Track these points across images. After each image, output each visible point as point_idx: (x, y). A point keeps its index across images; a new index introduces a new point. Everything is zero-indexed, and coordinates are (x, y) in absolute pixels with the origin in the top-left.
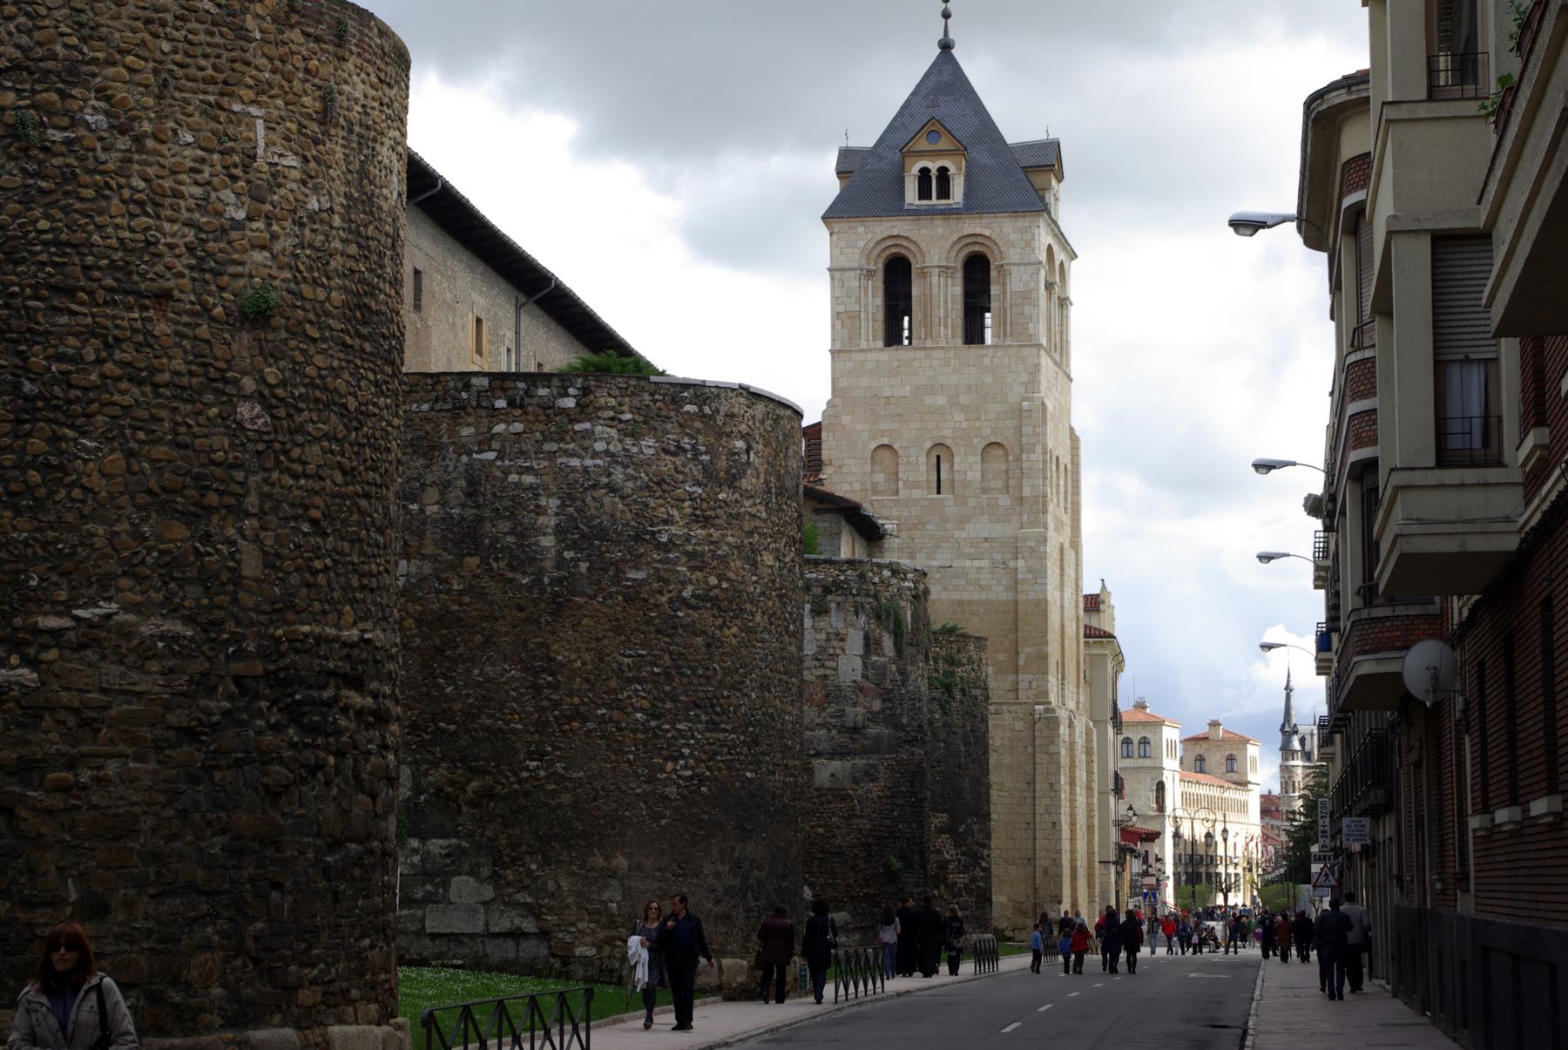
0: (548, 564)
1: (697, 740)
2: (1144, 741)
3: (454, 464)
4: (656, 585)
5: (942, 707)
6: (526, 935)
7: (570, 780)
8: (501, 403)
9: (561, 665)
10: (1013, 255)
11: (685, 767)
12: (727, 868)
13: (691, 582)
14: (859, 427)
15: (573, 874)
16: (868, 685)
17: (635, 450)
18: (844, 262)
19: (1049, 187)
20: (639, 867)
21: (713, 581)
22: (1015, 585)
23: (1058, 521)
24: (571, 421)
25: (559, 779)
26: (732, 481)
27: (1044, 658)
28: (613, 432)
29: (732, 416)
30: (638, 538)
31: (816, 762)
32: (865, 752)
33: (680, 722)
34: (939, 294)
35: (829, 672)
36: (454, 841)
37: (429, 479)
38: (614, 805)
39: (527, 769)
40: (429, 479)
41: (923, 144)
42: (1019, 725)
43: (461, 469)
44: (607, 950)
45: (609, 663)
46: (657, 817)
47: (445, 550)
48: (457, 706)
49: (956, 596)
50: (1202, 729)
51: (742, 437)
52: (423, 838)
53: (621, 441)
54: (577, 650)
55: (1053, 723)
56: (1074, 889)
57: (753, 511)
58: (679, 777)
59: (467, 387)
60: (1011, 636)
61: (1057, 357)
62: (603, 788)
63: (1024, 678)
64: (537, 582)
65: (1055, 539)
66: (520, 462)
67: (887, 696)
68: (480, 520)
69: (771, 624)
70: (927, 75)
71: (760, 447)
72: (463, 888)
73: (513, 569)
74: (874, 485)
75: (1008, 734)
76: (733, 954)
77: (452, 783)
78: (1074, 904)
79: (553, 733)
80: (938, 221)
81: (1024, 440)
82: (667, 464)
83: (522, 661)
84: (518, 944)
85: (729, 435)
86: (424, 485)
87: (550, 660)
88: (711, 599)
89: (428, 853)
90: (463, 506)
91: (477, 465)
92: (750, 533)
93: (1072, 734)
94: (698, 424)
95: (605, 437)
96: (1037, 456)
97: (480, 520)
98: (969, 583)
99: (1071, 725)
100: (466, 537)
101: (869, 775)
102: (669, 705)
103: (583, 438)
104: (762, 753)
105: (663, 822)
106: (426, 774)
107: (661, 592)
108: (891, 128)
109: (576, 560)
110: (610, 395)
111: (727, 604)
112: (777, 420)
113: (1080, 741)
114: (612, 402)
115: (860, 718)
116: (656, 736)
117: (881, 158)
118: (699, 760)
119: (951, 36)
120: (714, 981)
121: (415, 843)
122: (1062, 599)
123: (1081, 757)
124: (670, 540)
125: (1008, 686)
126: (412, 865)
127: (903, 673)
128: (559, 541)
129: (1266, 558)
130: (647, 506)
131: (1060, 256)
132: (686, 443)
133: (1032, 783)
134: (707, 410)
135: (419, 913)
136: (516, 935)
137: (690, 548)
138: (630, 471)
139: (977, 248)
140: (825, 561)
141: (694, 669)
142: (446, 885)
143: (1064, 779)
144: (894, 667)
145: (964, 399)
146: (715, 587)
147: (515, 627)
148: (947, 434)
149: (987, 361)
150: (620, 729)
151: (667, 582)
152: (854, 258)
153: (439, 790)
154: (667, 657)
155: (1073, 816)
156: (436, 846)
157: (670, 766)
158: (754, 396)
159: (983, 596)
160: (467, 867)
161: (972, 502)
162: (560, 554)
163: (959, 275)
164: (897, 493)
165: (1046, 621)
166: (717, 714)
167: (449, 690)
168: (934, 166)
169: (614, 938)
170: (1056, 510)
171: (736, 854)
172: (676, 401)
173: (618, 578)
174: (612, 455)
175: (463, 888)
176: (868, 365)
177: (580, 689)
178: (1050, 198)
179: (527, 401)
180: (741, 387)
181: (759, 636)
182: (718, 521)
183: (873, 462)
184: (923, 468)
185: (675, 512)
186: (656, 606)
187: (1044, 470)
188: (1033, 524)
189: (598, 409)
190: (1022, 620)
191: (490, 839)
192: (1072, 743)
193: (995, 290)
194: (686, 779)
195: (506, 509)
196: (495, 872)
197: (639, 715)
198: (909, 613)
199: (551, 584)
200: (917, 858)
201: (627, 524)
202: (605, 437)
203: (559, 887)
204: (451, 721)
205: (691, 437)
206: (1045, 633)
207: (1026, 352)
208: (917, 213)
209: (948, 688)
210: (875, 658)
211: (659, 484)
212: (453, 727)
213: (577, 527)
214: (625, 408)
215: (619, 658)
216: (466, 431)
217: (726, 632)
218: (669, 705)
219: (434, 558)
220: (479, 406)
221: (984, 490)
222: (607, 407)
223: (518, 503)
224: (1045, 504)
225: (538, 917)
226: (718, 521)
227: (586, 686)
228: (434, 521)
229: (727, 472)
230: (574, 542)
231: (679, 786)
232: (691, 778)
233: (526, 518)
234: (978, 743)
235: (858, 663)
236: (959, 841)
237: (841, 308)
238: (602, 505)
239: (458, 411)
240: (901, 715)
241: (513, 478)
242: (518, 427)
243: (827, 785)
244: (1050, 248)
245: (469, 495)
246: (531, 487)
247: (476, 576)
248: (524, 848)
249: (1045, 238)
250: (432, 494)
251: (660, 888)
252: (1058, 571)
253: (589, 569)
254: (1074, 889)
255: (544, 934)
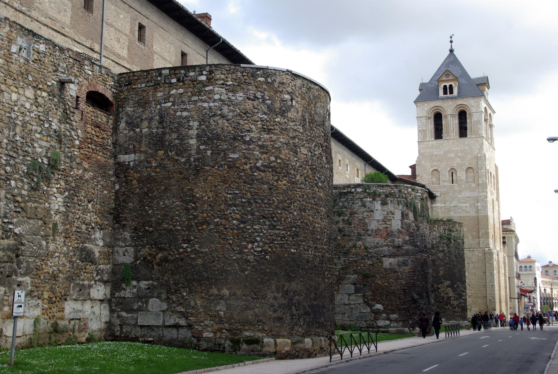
0: (193, 152)
1: (264, 234)
2: (530, 267)
3: (155, 109)
4: (243, 160)
5: (447, 245)
6: (182, 327)
7: (201, 252)
8: (174, 81)
9: (199, 199)
10: (473, 110)
11: (258, 246)
12: (280, 295)
13: (261, 159)
14: (427, 164)
15: (203, 298)
16: (403, 230)
17: (233, 98)
18: (421, 115)
19: (485, 90)
20: (234, 294)
21: (273, 159)
22: (478, 211)
23: (491, 192)
24: (204, 86)
25: (197, 252)
26: (283, 113)
27: (487, 234)
28: (223, 90)
29: (283, 83)
30: (235, 139)
31: (384, 259)
32: (403, 255)
33: (255, 225)
34: (451, 124)
35: (388, 226)
36: (151, 282)
37: (144, 117)
38: (222, 265)
39: (182, 248)
40: (144, 117)
41: (444, 78)
42: (480, 255)
43: (157, 111)
44: (218, 334)
45: (221, 197)
46: (243, 271)
47: (150, 148)
48: (153, 219)
49: (459, 215)
50: (547, 263)
51: (289, 93)
52: (138, 281)
53: (227, 94)
54: (206, 192)
55: (491, 254)
56: (500, 306)
57: (295, 128)
58: (255, 251)
59: (160, 75)
60: (477, 227)
61: (490, 142)
62: (217, 256)
63: (482, 240)
64: (188, 160)
65: (490, 198)
66: (182, 106)
67: (411, 235)
68: (164, 133)
69: (306, 181)
70: (446, 59)
71: (299, 99)
72: (155, 304)
73: (178, 155)
74: (432, 182)
75: (477, 257)
76: (283, 337)
77: (150, 255)
78: (501, 311)
79: (194, 231)
80: (450, 101)
81: (479, 166)
82: (249, 105)
83: (181, 198)
84: (178, 331)
85: (281, 92)
86: (142, 120)
87: (194, 196)
88: (271, 167)
89: (140, 287)
90: (157, 128)
91: (163, 109)
92: (294, 138)
93: (498, 258)
94: (265, 86)
95: (219, 93)
96: (483, 171)
97: (164, 133)
98: (463, 211)
99: (498, 255)
100: (158, 142)
101: (405, 263)
102: (250, 217)
103: (209, 93)
104: (301, 241)
105: (246, 273)
106: (139, 251)
107: (246, 164)
108: (435, 75)
109: (205, 150)
110: (222, 74)
111: (281, 170)
112: (309, 89)
113: (501, 260)
114: (223, 76)
115: (400, 243)
116: (243, 232)
117: (432, 84)
118: (265, 243)
119: (453, 48)
120: (272, 350)
121: (134, 283)
122: (494, 216)
123: (502, 265)
124: (250, 139)
125: (476, 243)
126: (133, 293)
127: (417, 226)
128: (198, 141)
129: (552, 140)
130: (239, 124)
131: (489, 111)
132: (259, 95)
133: (485, 273)
134: (269, 80)
135: (136, 315)
136: (177, 326)
137: (260, 143)
138: (231, 108)
139: (462, 108)
140: (386, 186)
141: (262, 200)
142: (147, 302)
143: (495, 272)
144: (414, 224)
145: (459, 154)
146: (274, 162)
147: (178, 182)
148: (455, 165)
149: (466, 142)
150: (226, 229)
151: (249, 159)
152: (424, 114)
153: (145, 258)
154: (249, 194)
155: (499, 283)
156: (143, 284)
157: (250, 246)
158: (296, 76)
159: (468, 215)
160: (156, 294)
161: (463, 186)
162: (198, 147)
163: (457, 117)
164: (439, 184)
165: (488, 222)
166: (275, 221)
167: (150, 212)
168: (448, 85)
169: (222, 329)
170: (490, 188)
171: (285, 288)
172: (254, 76)
173: (225, 157)
174: (223, 101)
175: (155, 304)
176: (429, 146)
177: (206, 210)
178: (485, 93)
179: (185, 78)
180: (287, 71)
181: (299, 186)
182: (275, 131)
183: (432, 175)
184: (447, 176)
185: (253, 127)
186: (244, 170)
187: (486, 175)
188: (483, 192)
189: (216, 80)
190: (480, 223)
191: (166, 281)
192: (498, 261)
193: (468, 121)
194: (258, 252)
195: (176, 128)
196: (168, 297)
197: (235, 222)
198: (419, 205)
199: (194, 161)
200: (425, 295)
201: (230, 132)
202: (219, 93)
203: (196, 304)
204: (151, 226)
205: (261, 92)
206: (487, 226)
207: (479, 139)
208: (443, 99)
209: (449, 239)
210: (406, 221)
211: (245, 114)
212: (151, 229)
213: (206, 134)
214: (229, 79)
215: (225, 195)
216: (159, 94)
217: (280, 183)
218: (250, 217)
219: (146, 152)
220: (165, 83)
221: (467, 182)
222: (220, 79)
223: (180, 125)
224: (486, 186)
225: (186, 318)
226: (275, 131)
227: (209, 208)
228: (146, 135)
229: (280, 109)
230: (205, 141)
231: (255, 255)
232: (261, 252)
233: (184, 131)
234: (461, 258)
235: (399, 223)
236: (454, 290)
237: (421, 129)
238: (218, 124)
239: (157, 85)
240: (417, 242)
241: (179, 114)
242: (181, 91)
243: (388, 267)
244: (485, 108)
245: (160, 123)
246: (186, 117)
247: (162, 159)
248: (181, 285)
249: (483, 105)
250: (145, 124)
251: (245, 304)
252: (492, 207)
253: (211, 153)
254: (500, 306)
255: (190, 326)
